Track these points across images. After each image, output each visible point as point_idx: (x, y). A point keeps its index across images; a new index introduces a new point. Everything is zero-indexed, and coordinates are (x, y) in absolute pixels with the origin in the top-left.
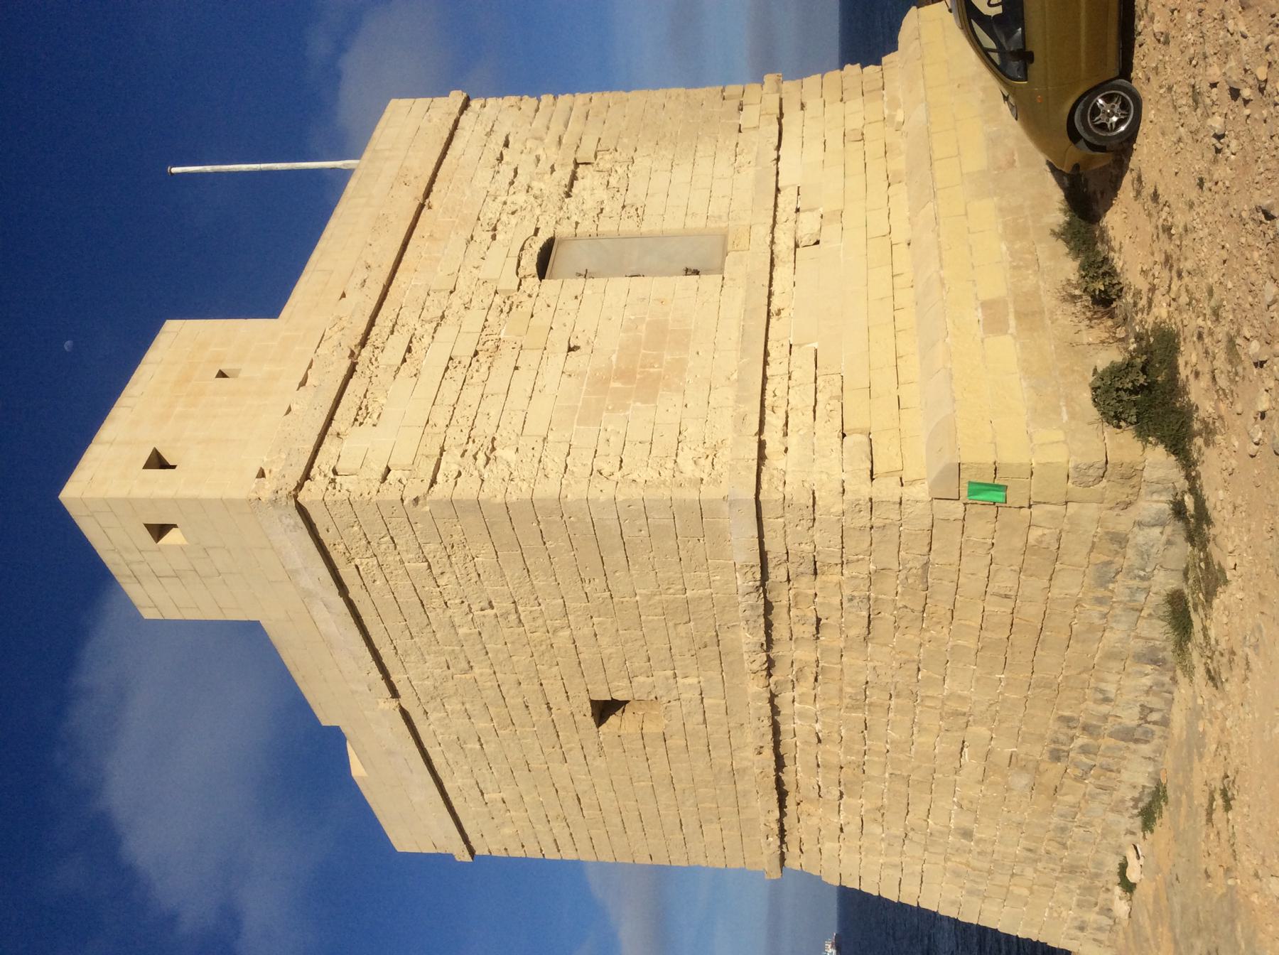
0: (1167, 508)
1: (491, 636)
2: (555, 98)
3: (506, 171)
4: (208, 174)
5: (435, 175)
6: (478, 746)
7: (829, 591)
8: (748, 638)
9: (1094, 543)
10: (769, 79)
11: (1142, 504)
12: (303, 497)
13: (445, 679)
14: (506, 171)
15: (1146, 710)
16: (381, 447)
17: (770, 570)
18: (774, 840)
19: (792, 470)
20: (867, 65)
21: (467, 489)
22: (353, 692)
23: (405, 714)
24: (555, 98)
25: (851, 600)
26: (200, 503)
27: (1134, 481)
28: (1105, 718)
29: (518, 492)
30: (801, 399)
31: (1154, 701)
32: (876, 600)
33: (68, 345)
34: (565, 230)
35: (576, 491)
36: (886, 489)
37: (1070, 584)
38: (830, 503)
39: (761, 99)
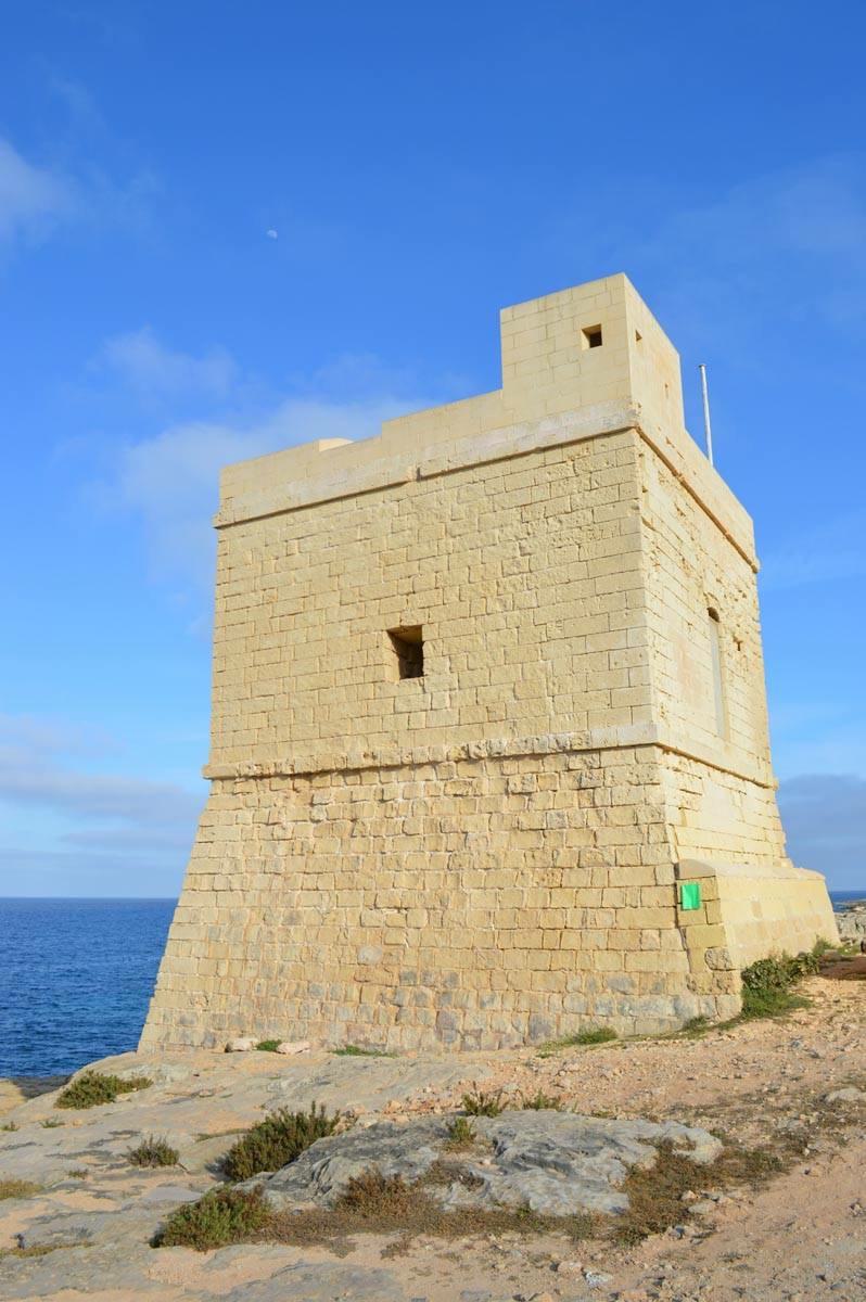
0: (696, 1014)
1: (493, 553)
2: (759, 632)
4: (702, 390)
5: (733, 544)
6: (359, 538)
7: (567, 800)
9: (651, 972)
11: (695, 998)
12: (634, 433)
13: (440, 517)
15: (478, 1034)
17: (579, 757)
18: (256, 771)
20: (786, 848)
22: (423, 449)
24: (759, 632)
25: (558, 815)
27: (716, 990)
28: (464, 1007)
31: (486, 1040)
32: (561, 834)
33: (273, 234)
37: (606, 963)
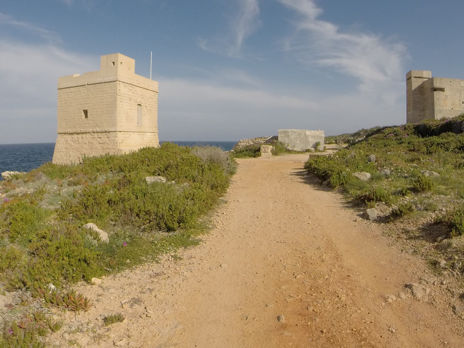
3: (149, 99)
8: (98, 130)
10: (158, 131)
14: (149, 99)
16: (122, 89)
19: (119, 134)
21: (118, 99)
23: (85, 85)
26: (117, 69)
29: (118, 105)
30: (126, 136)
34: (142, 107)
35: (117, 112)
36: (118, 144)
38: (117, 139)
39: (156, 130)
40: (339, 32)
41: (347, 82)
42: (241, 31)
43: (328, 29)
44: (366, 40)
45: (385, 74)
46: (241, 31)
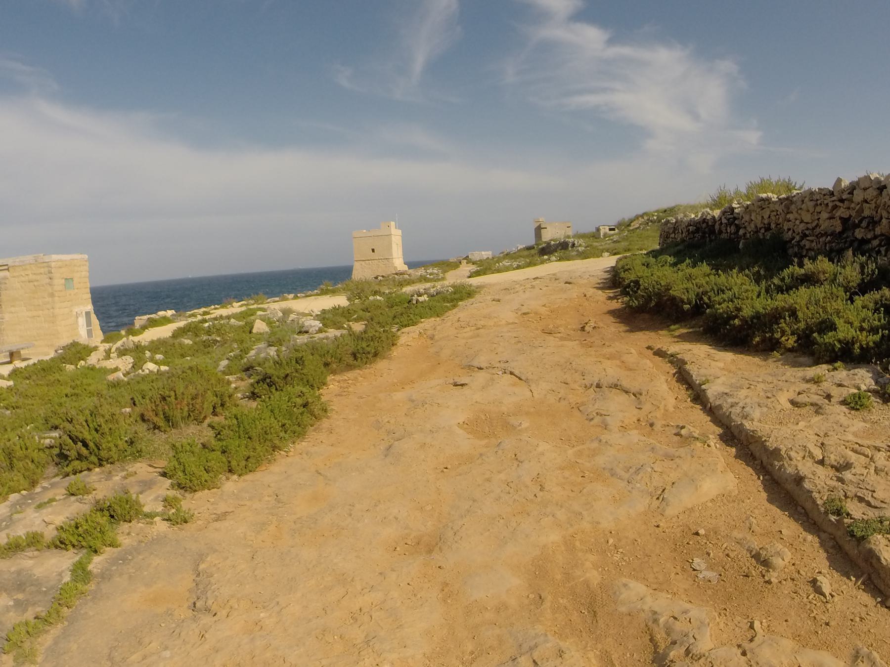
16: (393, 238)
40: (611, 42)
41: (621, 136)
42: (422, 47)
43: (592, 37)
44: (667, 58)
45: (696, 117)
46: (422, 47)
